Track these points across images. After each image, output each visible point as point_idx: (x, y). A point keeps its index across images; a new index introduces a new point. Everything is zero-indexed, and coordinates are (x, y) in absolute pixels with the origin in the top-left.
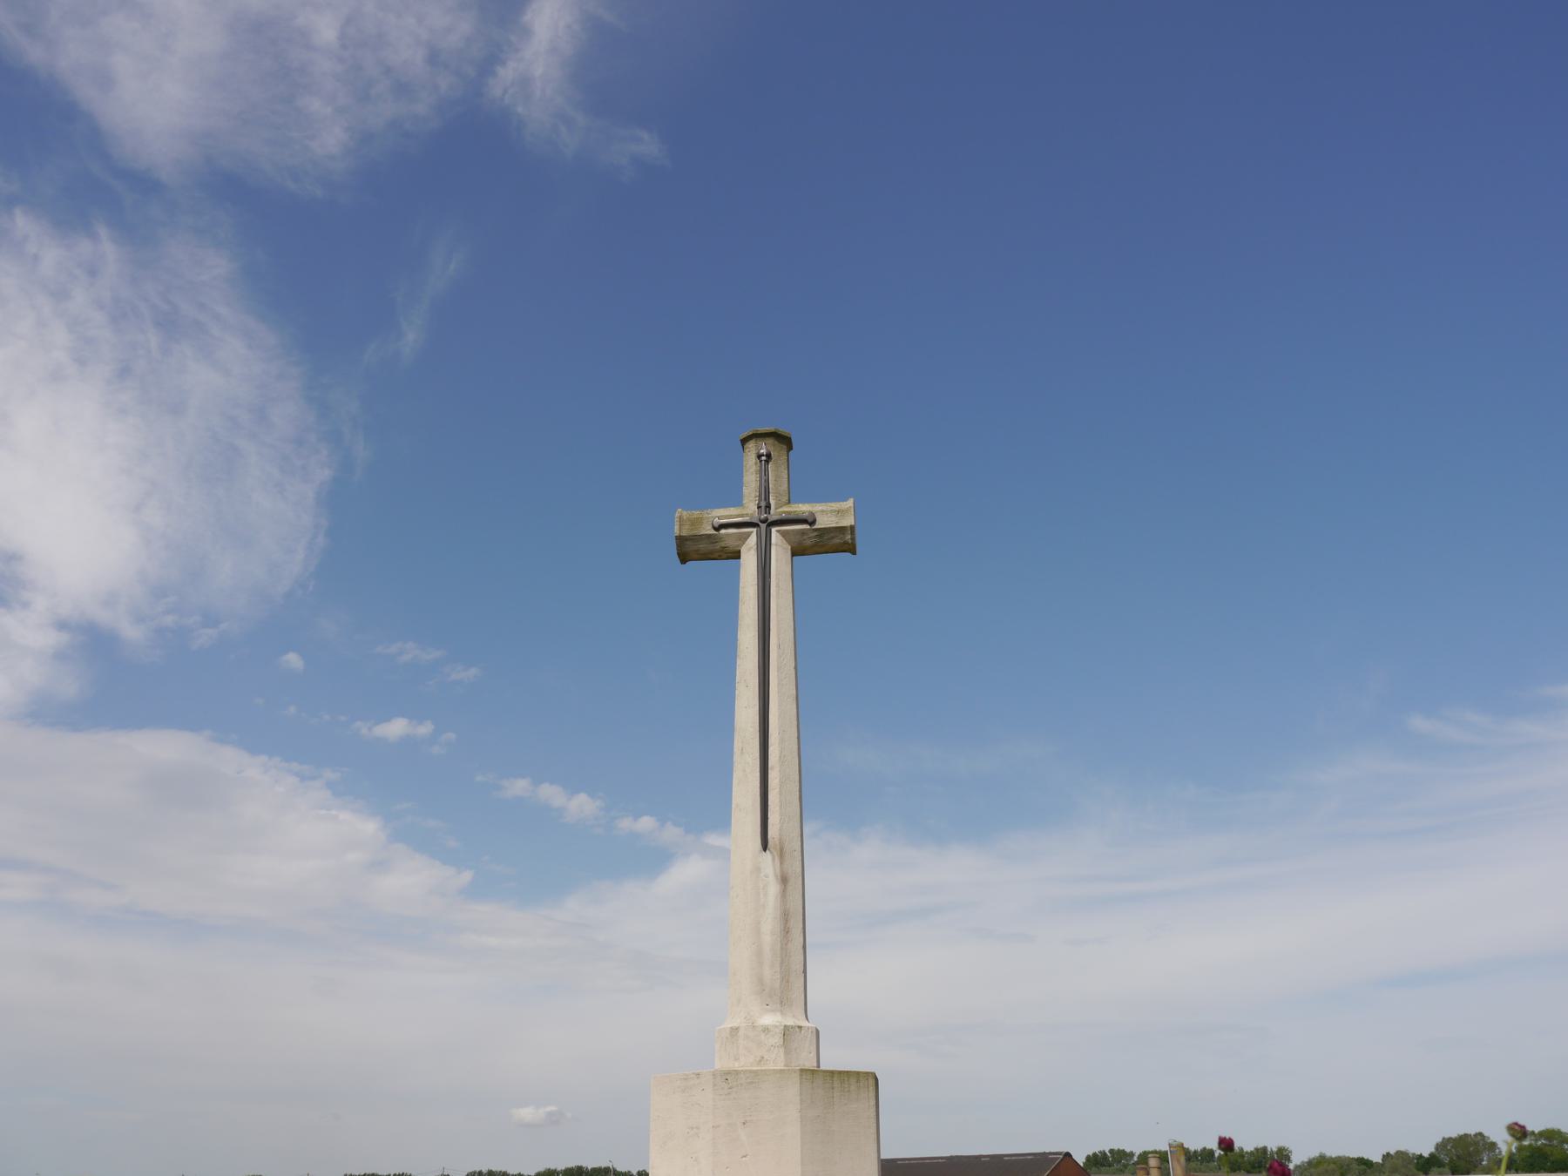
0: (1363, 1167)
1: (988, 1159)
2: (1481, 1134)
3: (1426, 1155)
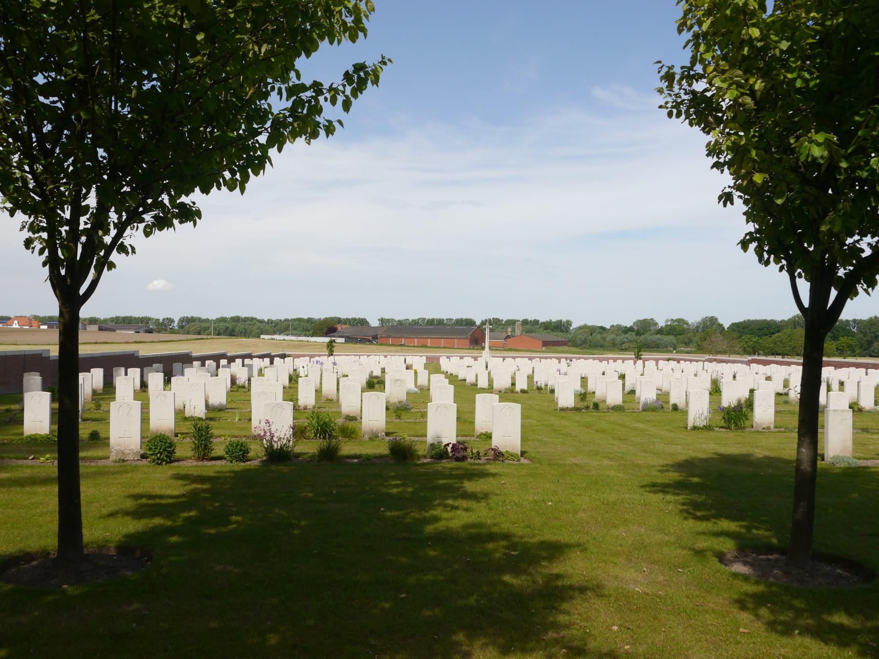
0: (601, 330)
1: (82, 290)
2: (652, 319)
3: (628, 326)
